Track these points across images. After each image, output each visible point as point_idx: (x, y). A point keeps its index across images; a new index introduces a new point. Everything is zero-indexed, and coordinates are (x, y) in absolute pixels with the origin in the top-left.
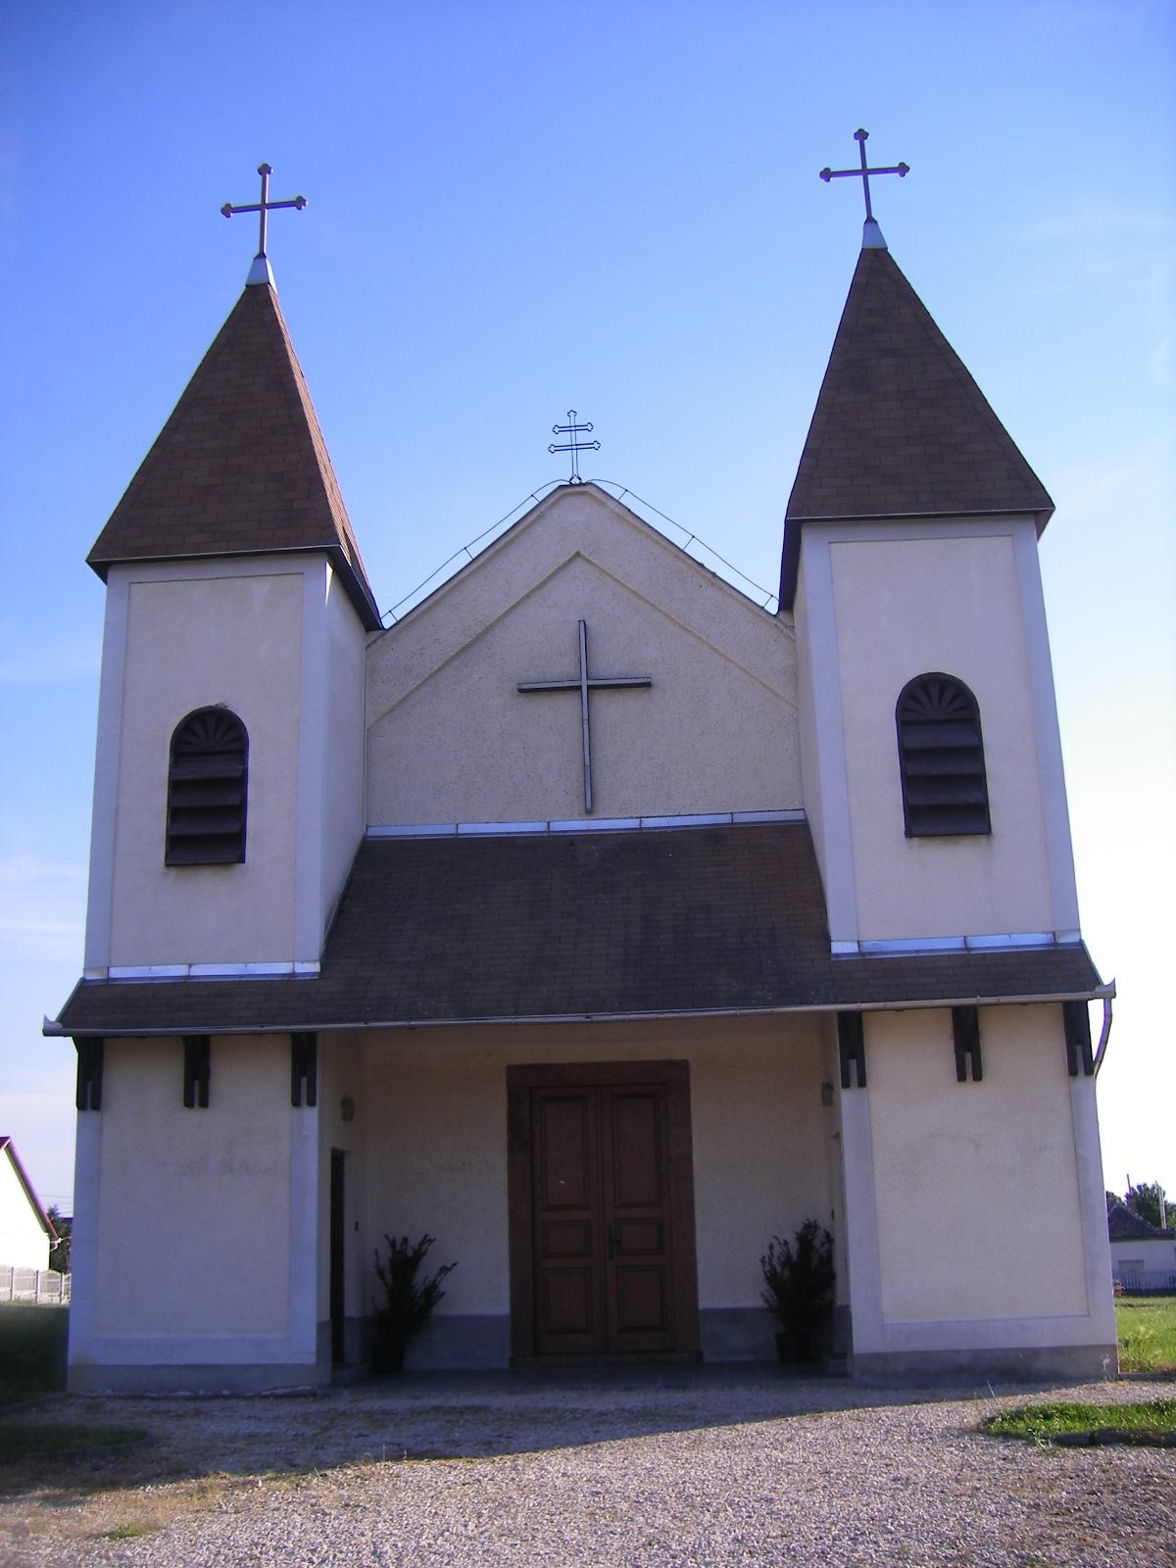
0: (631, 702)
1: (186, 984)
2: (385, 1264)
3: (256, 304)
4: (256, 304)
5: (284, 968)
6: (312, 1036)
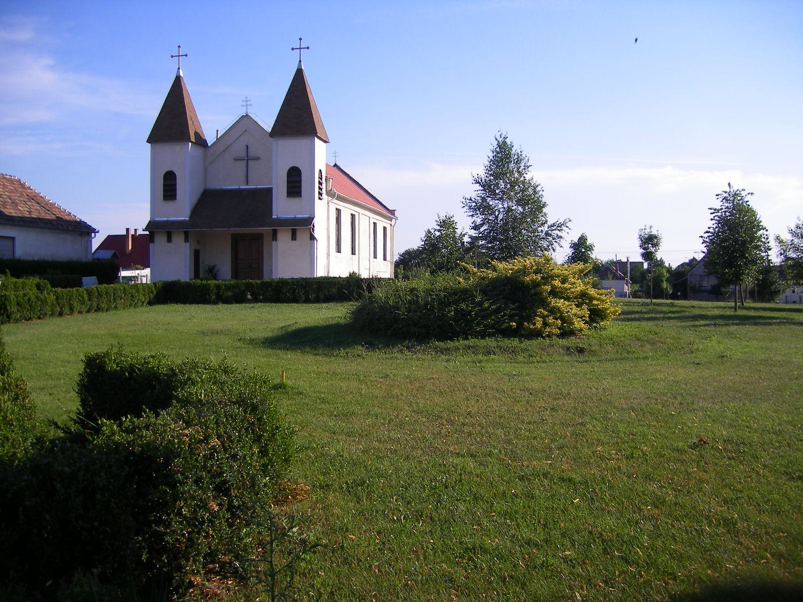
0: (256, 162)
1: (167, 222)
2: (207, 270)
3: (178, 81)
4: (178, 81)
5: (183, 219)
6: (188, 231)
